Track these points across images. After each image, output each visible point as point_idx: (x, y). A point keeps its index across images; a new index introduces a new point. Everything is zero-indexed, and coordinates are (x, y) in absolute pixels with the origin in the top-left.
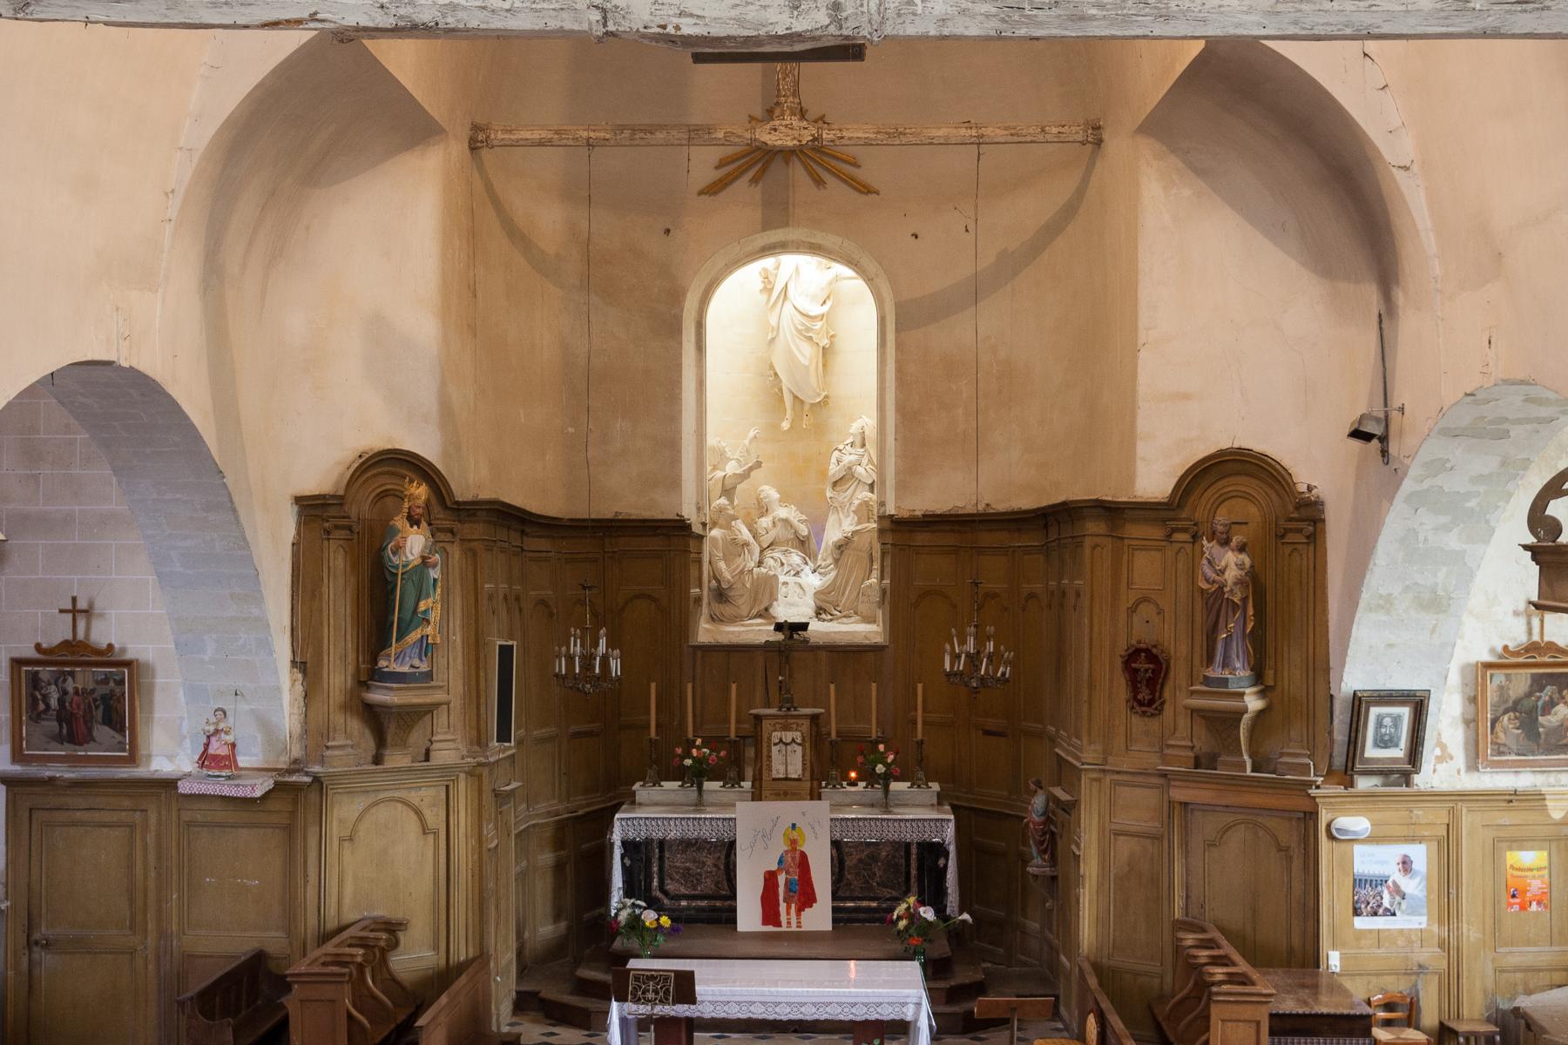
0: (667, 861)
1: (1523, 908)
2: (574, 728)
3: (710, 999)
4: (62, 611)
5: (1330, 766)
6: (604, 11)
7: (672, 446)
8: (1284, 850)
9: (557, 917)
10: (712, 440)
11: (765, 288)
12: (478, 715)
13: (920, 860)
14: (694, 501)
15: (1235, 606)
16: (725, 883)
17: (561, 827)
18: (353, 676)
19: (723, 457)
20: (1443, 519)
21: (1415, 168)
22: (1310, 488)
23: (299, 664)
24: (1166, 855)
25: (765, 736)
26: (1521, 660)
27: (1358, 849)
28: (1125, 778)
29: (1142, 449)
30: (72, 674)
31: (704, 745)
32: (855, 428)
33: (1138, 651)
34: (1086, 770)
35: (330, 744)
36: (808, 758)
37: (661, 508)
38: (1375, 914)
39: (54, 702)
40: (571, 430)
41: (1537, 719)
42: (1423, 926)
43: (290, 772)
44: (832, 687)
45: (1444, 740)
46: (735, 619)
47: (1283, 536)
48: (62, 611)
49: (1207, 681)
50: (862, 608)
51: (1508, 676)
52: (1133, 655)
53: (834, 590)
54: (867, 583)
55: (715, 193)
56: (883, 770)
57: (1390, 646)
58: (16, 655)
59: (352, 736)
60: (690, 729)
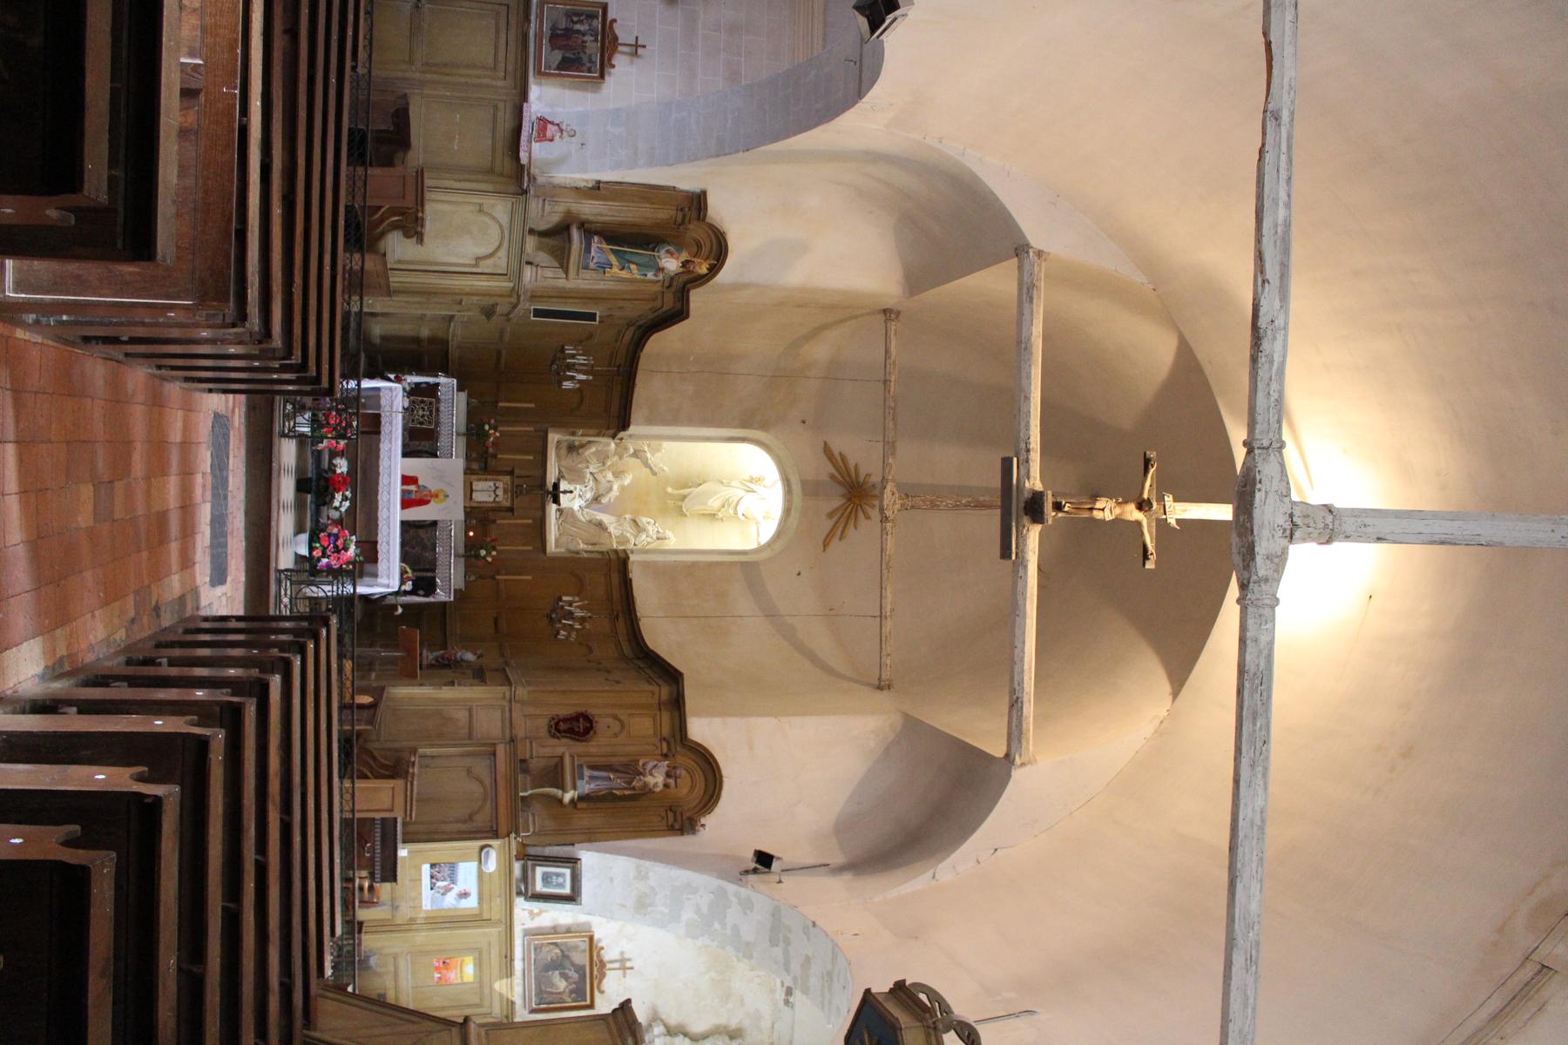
1: (437, 969)
2: (504, 352)
3: (393, 448)
4: (637, 38)
5: (528, 845)
6: (1268, 448)
7: (674, 420)
8: (471, 818)
9: (384, 338)
10: (666, 445)
11: (753, 479)
12: (551, 297)
14: (637, 433)
15: (630, 783)
17: (444, 342)
18: (588, 219)
19: (655, 451)
20: (705, 910)
21: (934, 882)
22: (703, 826)
23: (598, 185)
24: (459, 742)
25: (501, 477)
26: (595, 958)
27: (475, 864)
28: (507, 715)
29: (717, 721)
30: (596, 40)
32: (669, 533)
33: (591, 722)
34: (511, 690)
35: (547, 202)
36: (485, 505)
37: (637, 413)
38: (432, 877)
39: (577, 27)
40: (692, 359)
41: (557, 969)
42: (424, 908)
43: (529, 174)
44: (530, 521)
45: (544, 914)
46: (558, 456)
47: (671, 810)
48: (637, 38)
49: (581, 766)
51: (584, 951)
52: (587, 718)
54: (580, 542)
55: (825, 451)
56: (482, 555)
57: (612, 880)
58: (609, 6)
59: (549, 216)
60: (506, 429)
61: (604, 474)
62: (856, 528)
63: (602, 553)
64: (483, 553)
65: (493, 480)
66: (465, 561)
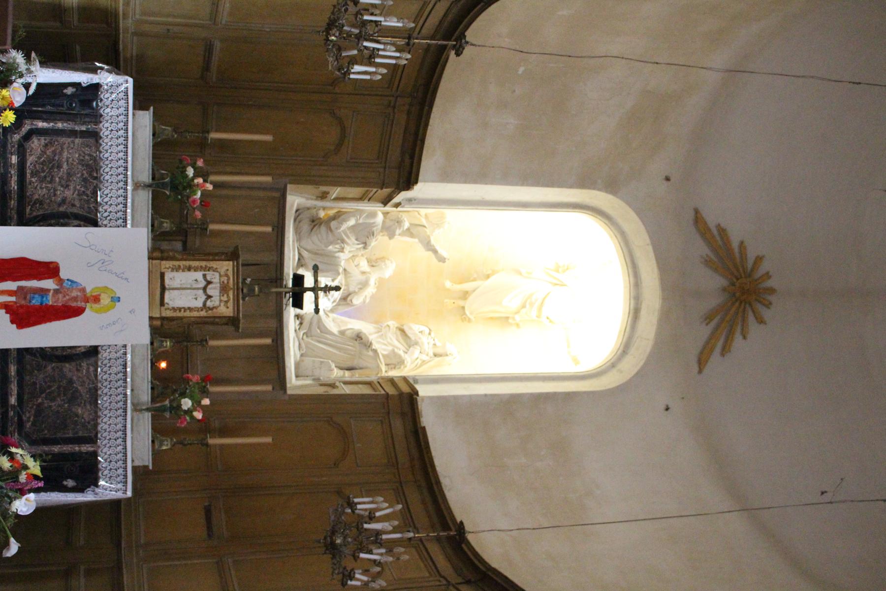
0: (69, 140)
2: (218, 45)
13: (73, 456)
16: (41, 212)
25: (214, 264)
31: (205, 194)
36: (188, 314)
37: (429, 163)
46: (297, 231)
50: (308, 361)
53: (321, 332)
56: (185, 407)
61: (356, 263)
62: (745, 338)
63: (369, 384)
64: (187, 404)
65: (201, 268)
66: (153, 417)
